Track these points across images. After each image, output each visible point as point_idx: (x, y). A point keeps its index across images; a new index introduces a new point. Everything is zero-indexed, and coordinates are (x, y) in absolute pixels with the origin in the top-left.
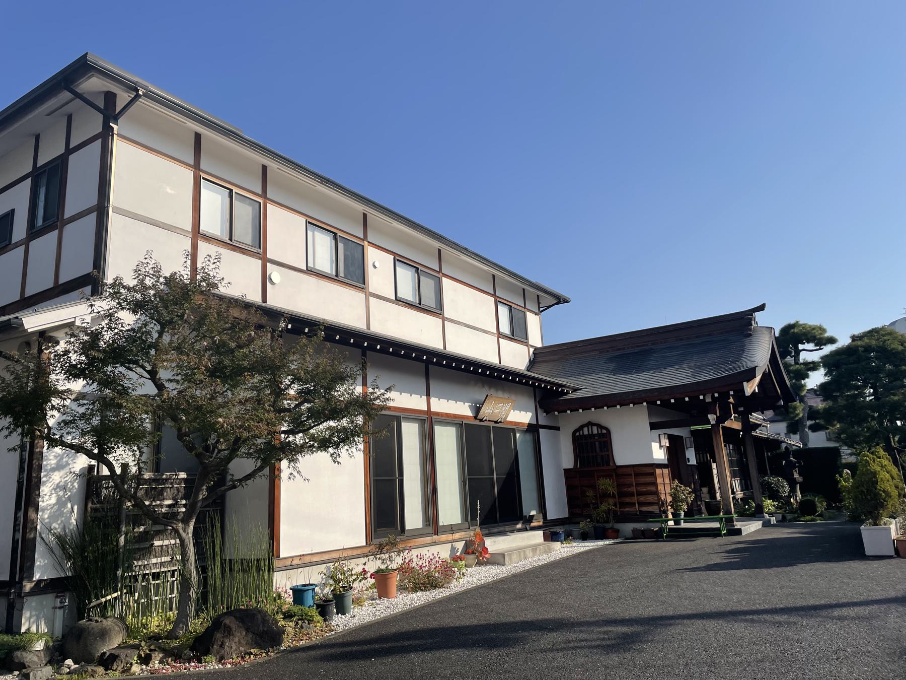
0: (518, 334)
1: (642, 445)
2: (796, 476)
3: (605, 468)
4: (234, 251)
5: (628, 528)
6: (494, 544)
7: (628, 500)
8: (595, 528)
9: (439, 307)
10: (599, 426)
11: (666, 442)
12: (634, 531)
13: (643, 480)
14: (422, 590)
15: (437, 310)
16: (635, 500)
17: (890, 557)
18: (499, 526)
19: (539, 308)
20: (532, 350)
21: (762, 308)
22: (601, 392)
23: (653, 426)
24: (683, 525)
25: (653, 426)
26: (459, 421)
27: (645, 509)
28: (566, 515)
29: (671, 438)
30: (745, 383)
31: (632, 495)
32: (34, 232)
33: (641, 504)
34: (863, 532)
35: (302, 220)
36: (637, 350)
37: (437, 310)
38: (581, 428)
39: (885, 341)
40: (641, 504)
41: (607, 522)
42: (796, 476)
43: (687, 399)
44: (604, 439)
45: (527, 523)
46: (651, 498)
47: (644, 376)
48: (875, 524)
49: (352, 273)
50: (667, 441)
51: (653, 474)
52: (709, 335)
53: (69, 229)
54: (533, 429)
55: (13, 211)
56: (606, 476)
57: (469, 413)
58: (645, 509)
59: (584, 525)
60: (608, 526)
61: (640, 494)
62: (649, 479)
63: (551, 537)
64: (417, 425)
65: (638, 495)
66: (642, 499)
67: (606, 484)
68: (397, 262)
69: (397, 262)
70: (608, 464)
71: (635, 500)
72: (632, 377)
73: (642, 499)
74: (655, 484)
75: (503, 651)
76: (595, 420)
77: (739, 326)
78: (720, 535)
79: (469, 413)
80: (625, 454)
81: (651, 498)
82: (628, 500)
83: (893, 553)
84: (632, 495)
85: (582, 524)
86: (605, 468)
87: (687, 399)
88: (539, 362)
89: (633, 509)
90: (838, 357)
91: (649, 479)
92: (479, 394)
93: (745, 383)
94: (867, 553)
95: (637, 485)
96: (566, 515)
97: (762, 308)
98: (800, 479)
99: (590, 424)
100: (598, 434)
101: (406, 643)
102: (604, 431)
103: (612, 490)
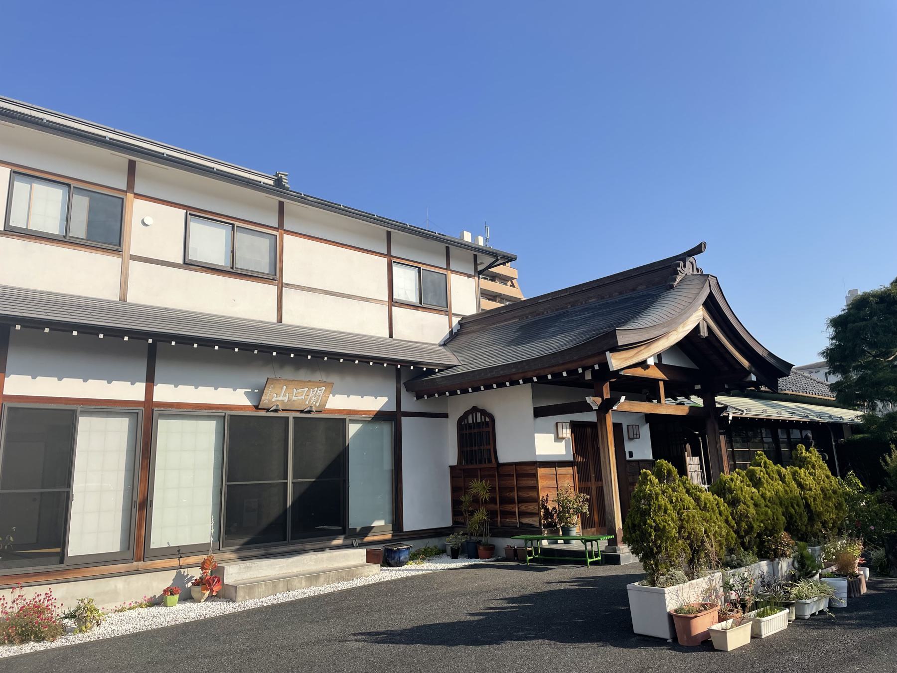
0: (432, 298)
3: (487, 465)
6: (236, 572)
9: (273, 273)
10: (484, 412)
11: (566, 433)
15: (273, 275)
17: (657, 642)
18: (289, 544)
19: (476, 269)
20: (455, 321)
25: (539, 413)
26: (221, 413)
27: (526, 520)
28: (449, 523)
29: (575, 427)
30: (608, 353)
34: (632, 597)
37: (273, 275)
38: (466, 414)
40: (523, 514)
45: (356, 537)
46: (532, 507)
49: (105, 233)
50: (569, 431)
51: (534, 476)
54: (389, 418)
57: (246, 402)
58: (526, 520)
62: (531, 483)
63: (372, 558)
64: (127, 420)
65: (519, 503)
66: (523, 507)
68: (189, 217)
69: (189, 217)
70: (490, 461)
73: (523, 507)
74: (535, 488)
76: (481, 406)
79: (246, 402)
80: (508, 452)
81: (532, 507)
82: (509, 507)
86: (487, 465)
88: (467, 333)
89: (513, 520)
91: (531, 483)
92: (259, 377)
93: (608, 353)
94: (638, 628)
96: (449, 523)
97: (698, 250)
99: (475, 410)
102: (487, 419)
103: (485, 495)
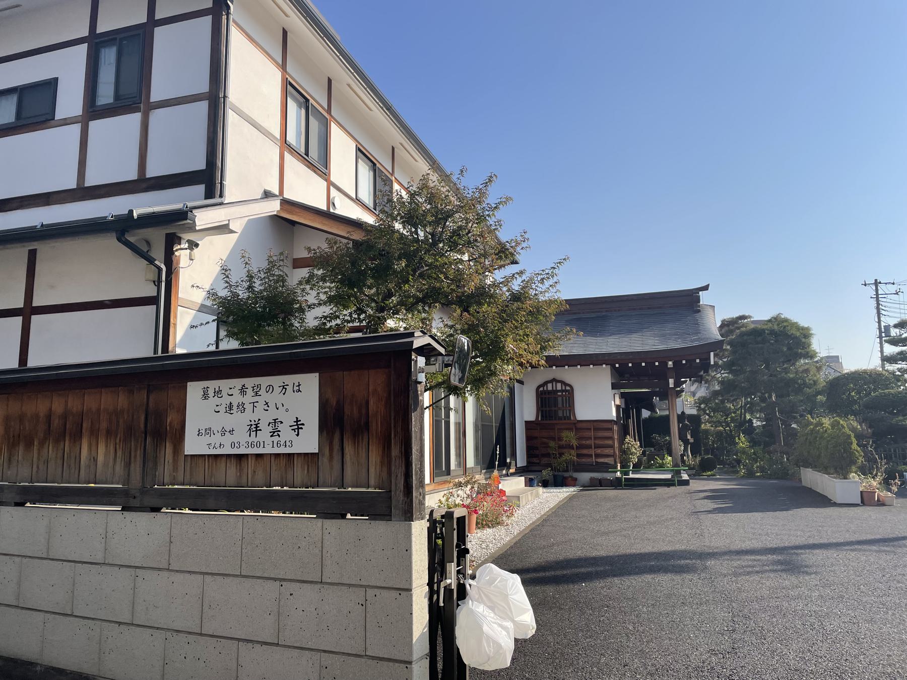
1: (597, 400)
2: (689, 437)
4: (309, 167)
5: (585, 477)
7: (585, 451)
8: (555, 476)
10: (563, 383)
12: (592, 479)
13: (601, 434)
14: (489, 527)
16: (592, 452)
21: (706, 288)
22: (575, 352)
23: (614, 386)
24: (631, 476)
31: (589, 447)
32: (93, 110)
33: (597, 456)
35: (353, 145)
36: (593, 315)
38: (546, 383)
39: (785, 327)
40: (597, 456)
41: (567, 471)
42: (689, 437)
43: (643, 364)
44: (569, 393)
46: (607, 451)
47: (611, 340)
48: (845, 478)
52: (660, 308)
53: (156, 116)
55: (56, 80)
56: (570, 429)
59: (546, 473)
60: (566, 474)
61: (597, 447)
66: (599, 451)
67: (569, 437)
71: (592, 452)
72: (599, 339)
73: (599, 451)
75: (677, 578)
76: (558, 377)
77: (685, 303)
78: (673, 485)
81: (607, 451)
82: (585, 451)
83: (859, 502)
84: (589, 447)
85: (544, 472)
87: (657, 364)
89: (589, 460)
90: (745, 337)
95: (595, 438)
97: (706, 288)
98: (692, 440)
99: (554, 380)
100: (562, 391)
101: (559, 573)
102: (568, 388)
103: (575, 443)
